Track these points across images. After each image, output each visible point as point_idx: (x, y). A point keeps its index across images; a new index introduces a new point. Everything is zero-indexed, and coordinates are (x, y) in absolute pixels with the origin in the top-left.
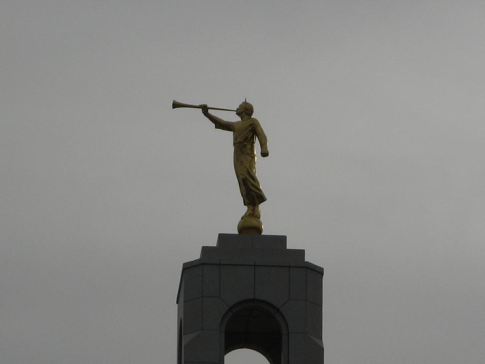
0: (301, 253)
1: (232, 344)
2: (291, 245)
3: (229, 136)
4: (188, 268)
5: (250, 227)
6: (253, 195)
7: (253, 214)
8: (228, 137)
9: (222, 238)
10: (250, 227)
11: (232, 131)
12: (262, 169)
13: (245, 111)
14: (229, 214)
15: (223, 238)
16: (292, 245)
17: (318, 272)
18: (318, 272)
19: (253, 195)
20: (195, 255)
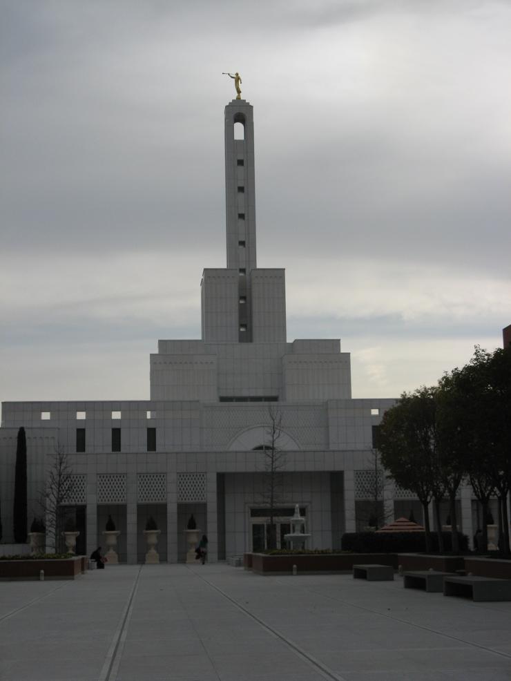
0: (249, 103)
1: (236, 121)
2: (460, 369)
3: (234, 80)
4: (226, 107)
5: (238, 98)
6: (239, 92)
7: (239, 95)
8: (234, 80)
9: (233, 101)
10: (238, 98)
11: (354, 400)
12: (241, 86)
13: (237, 74)
14: (234, 96)
15: (230, 103)
16: (250, 104)
17: (252, 107)
18: (252, 107)
19: (239, 92)
20: (228, 104)
